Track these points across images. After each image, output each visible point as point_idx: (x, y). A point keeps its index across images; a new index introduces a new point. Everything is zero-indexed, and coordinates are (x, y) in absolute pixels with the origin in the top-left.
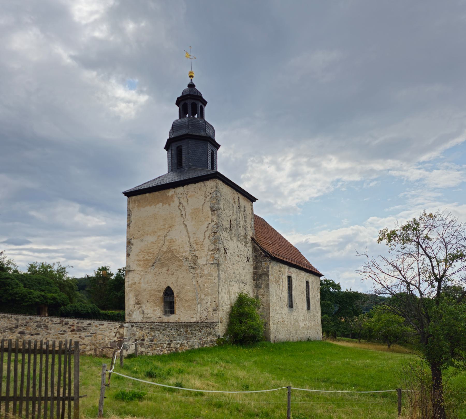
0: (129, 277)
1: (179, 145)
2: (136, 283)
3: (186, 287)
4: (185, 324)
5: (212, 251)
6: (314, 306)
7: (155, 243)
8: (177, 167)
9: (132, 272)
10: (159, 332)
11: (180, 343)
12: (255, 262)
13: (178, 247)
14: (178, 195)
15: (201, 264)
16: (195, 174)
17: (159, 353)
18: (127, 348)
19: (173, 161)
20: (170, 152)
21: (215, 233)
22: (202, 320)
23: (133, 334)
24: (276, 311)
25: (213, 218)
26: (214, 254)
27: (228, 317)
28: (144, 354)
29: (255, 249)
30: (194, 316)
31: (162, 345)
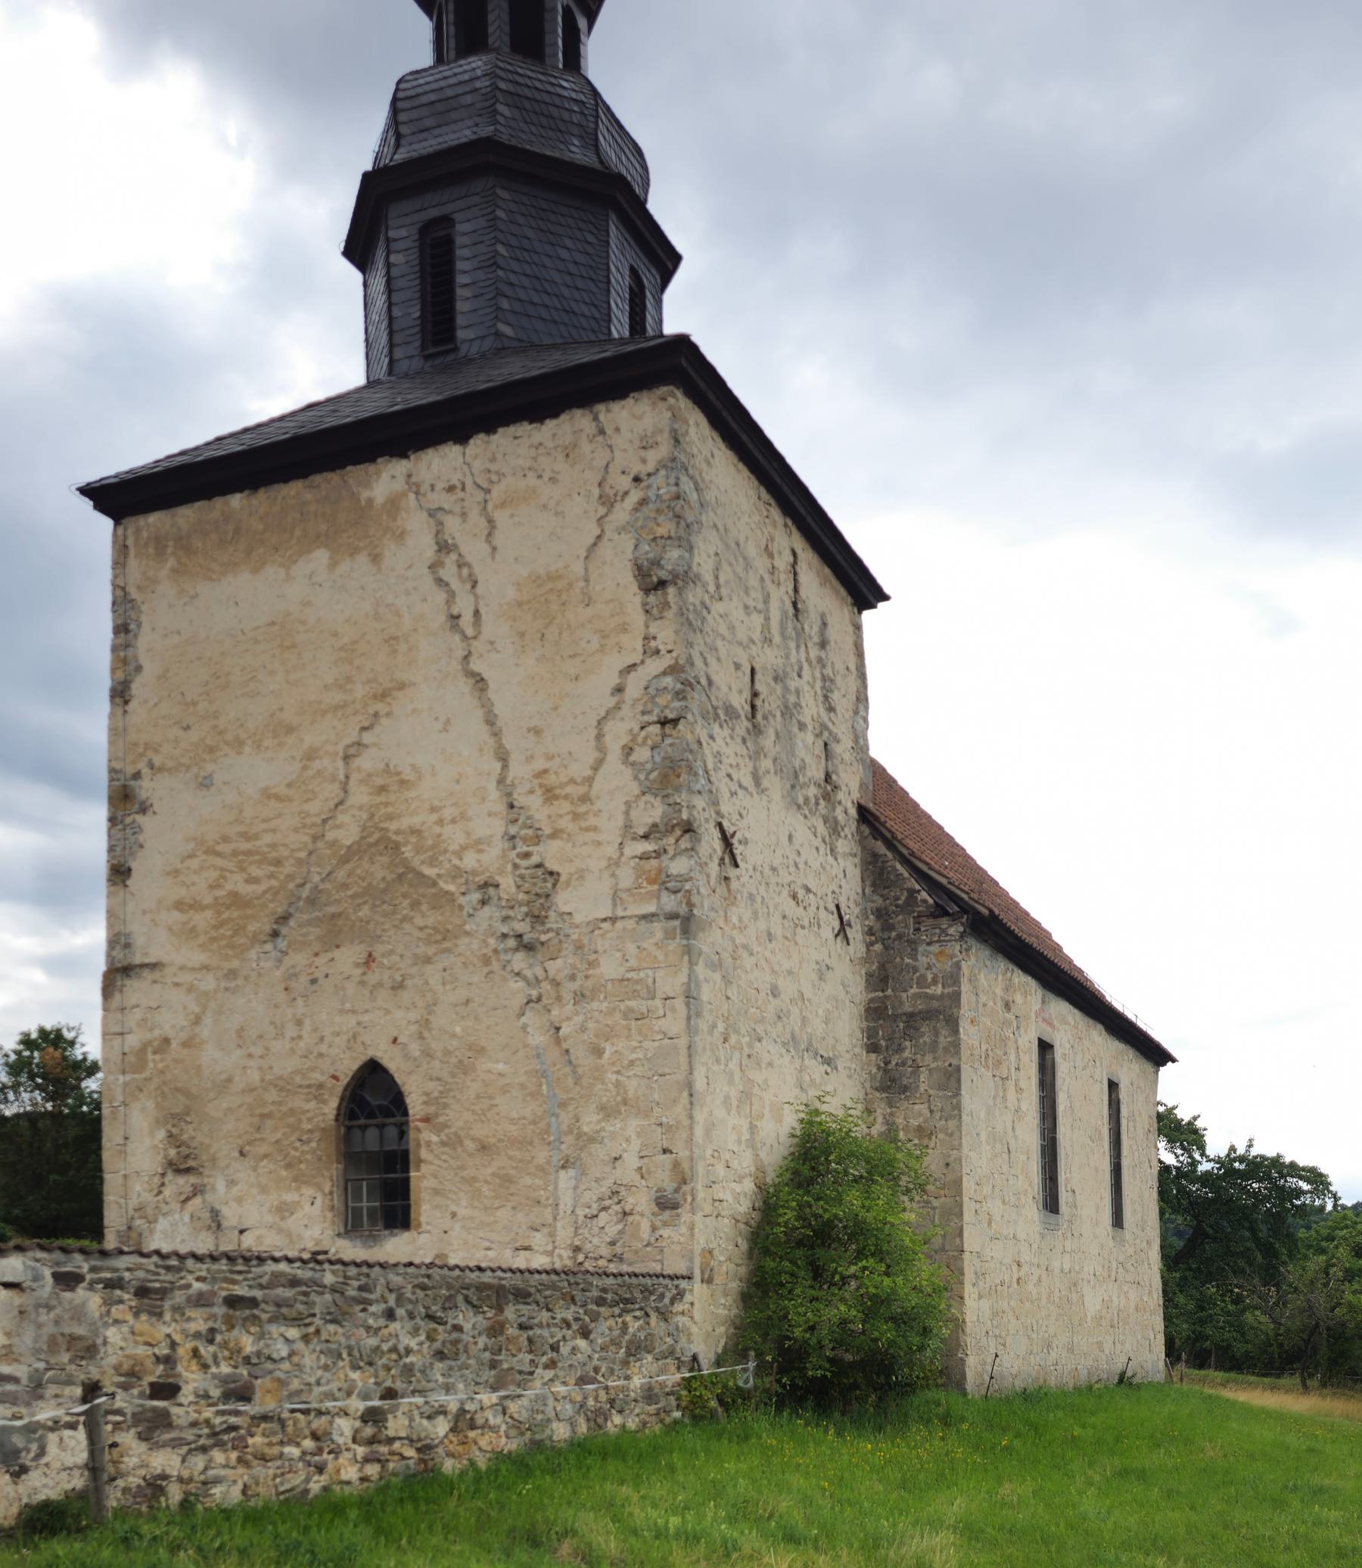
0: (123, 1009)
1: (433, 213)
2: (167, 1041)
3: (484, 1065)
4: (487, 1278)
5: (646, 837)
6: (1139, 1209)
7: (289, 799)
8: (423, 347)
9: (146, 973)
10: (293, 1333)
11: (453, 1407)
12: (878, 947)
13: (435, 817)
14: (431, 496)
15: (578, 918)
16: (541, 364)
17: (296, 1480)
18: (17, 1452)
19: (397, 312)
20: (379, 283)
21: (663, 723)
22: (589, 1265)
23: (73, 1339)
24: (990, 1223)
25: (653, 630)
26: (658, 854)
27: (744, 1246)
28: (175, 1494)
29: (875, 874)
30: (538, 1240)
31: (320, 1423)
